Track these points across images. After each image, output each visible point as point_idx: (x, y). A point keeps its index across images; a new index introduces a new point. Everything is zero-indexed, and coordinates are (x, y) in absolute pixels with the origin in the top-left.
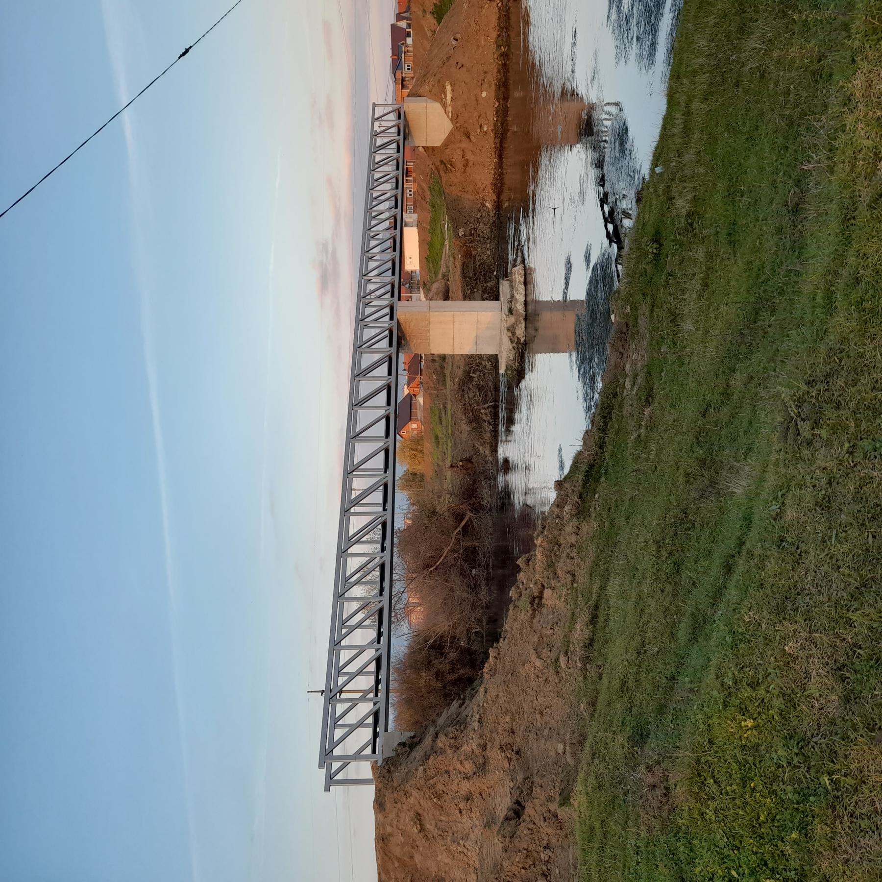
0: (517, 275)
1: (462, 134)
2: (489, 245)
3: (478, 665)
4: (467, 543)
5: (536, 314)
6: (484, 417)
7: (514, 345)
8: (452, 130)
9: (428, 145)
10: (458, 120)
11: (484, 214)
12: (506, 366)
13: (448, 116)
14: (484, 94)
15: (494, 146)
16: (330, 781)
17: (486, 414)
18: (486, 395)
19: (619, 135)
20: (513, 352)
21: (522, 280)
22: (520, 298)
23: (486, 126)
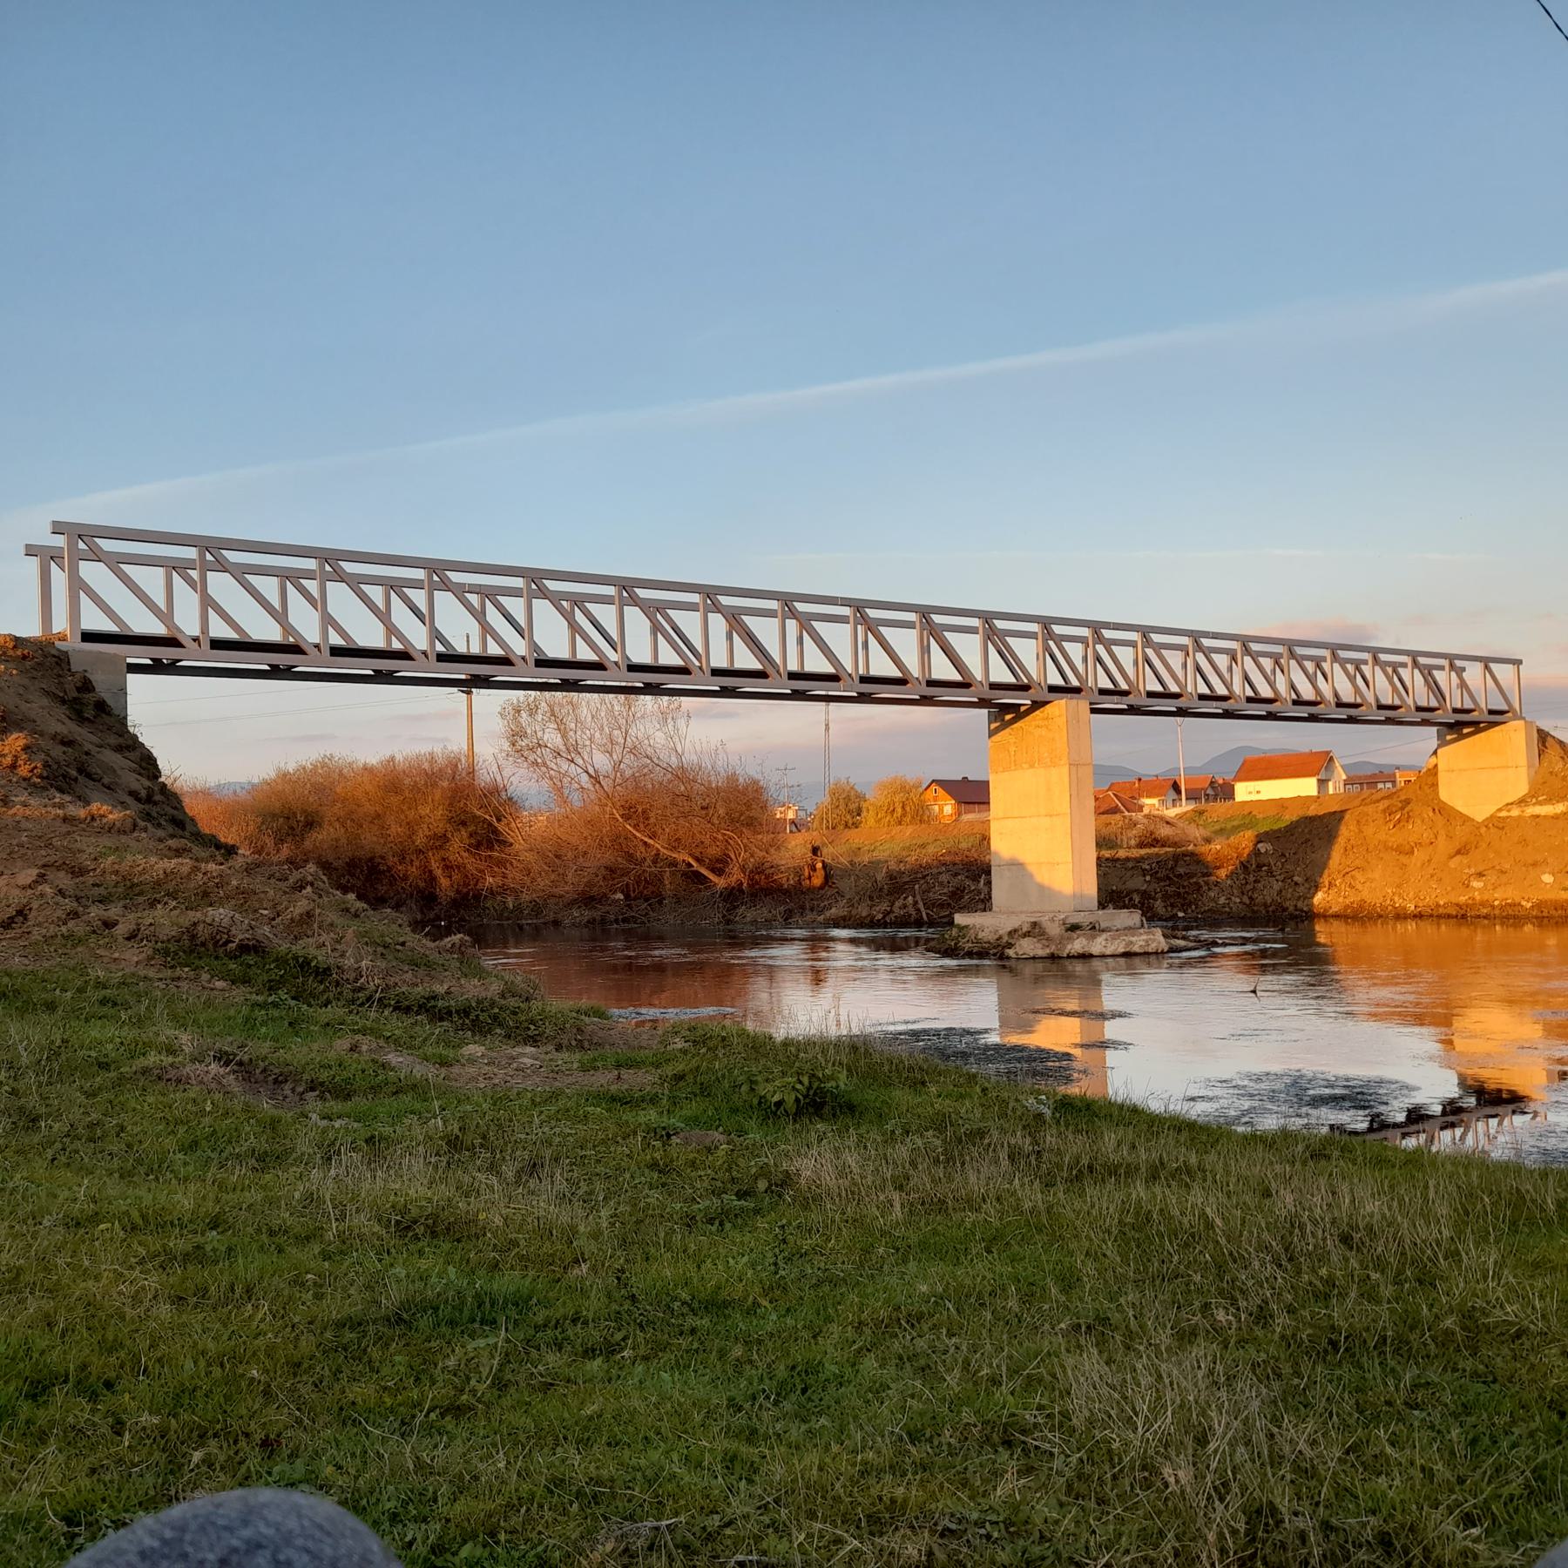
0: (1145, 937)
1: (1464, 839)
2: (1238, 900)
3: (458, 912)
5: (1068, 979)
7: (1006, 938)
9: (1440, 774)
10: (1493, 830)
11: (1301, 889)
12: (967, 927)
13: (1500, 810)
14: (1548, 878)
15: (1442, 903)
16: (46, 556)
17: (905, 906)
18: (942, 906)
19: (1362, 1093)
20: (992, 938)
21: (1136, 949)
22: (1098, 945)
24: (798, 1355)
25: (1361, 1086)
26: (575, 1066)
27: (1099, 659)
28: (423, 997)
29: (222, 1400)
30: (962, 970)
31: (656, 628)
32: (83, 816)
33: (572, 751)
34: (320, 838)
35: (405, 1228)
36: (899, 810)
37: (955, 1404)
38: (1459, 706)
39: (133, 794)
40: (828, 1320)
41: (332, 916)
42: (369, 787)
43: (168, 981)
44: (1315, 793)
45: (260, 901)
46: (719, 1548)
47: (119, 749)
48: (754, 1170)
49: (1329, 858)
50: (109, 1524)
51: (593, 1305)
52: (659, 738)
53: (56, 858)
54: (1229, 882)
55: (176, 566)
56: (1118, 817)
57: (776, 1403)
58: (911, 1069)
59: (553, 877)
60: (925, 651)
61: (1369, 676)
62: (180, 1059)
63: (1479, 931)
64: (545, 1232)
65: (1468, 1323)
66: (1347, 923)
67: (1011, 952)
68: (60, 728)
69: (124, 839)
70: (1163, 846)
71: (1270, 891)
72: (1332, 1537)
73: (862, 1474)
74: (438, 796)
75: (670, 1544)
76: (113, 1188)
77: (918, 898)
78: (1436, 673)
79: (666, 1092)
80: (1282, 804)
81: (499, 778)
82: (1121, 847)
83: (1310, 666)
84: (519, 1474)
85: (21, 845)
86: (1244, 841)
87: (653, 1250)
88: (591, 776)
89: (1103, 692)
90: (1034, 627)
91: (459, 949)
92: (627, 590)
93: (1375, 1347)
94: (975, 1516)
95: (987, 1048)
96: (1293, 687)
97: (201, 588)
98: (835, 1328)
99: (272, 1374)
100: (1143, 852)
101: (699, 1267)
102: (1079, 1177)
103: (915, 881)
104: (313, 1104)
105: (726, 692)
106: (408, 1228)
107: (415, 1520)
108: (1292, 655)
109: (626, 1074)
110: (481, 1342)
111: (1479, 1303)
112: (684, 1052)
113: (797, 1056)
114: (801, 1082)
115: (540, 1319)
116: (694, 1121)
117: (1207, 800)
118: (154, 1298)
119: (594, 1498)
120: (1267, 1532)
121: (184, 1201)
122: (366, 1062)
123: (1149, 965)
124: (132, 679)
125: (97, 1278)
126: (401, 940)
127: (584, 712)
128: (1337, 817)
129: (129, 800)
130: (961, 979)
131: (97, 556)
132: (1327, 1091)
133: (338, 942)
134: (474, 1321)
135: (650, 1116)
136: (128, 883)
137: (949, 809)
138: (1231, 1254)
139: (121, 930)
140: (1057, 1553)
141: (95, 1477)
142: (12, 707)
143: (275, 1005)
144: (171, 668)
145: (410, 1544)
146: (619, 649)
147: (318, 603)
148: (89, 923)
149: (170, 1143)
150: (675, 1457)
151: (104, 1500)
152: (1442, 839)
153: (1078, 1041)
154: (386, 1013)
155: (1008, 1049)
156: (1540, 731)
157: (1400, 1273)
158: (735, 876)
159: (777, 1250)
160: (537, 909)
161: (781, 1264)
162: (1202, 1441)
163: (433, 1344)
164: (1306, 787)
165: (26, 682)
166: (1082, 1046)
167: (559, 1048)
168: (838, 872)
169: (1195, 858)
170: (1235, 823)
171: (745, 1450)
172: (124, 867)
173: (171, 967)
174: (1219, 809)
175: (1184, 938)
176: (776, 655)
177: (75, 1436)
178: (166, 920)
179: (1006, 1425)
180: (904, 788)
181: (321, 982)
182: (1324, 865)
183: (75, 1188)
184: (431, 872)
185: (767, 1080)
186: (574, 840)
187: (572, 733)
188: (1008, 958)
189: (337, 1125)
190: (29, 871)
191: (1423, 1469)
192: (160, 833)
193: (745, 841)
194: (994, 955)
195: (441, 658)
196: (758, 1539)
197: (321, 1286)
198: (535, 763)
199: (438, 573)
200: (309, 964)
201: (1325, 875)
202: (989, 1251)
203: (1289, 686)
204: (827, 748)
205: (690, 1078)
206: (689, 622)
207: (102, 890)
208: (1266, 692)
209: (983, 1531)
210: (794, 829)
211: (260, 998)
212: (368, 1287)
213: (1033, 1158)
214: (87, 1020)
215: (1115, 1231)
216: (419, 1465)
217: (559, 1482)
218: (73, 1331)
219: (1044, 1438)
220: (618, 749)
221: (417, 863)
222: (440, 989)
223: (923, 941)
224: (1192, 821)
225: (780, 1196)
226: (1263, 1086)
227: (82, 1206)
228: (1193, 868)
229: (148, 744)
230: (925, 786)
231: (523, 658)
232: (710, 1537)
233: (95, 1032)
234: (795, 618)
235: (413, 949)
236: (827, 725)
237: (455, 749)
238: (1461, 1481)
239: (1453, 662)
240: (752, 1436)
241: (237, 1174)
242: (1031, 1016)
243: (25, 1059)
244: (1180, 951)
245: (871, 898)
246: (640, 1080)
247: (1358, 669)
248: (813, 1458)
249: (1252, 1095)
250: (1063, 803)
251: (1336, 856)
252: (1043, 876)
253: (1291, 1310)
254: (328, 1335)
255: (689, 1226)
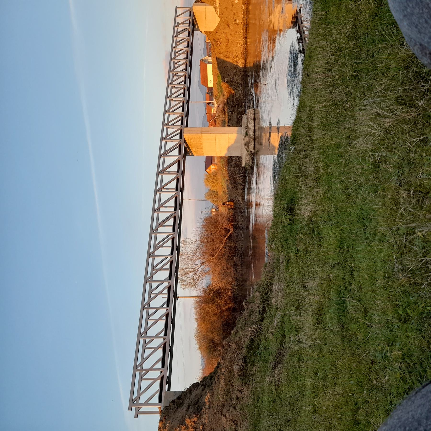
0: (250, 114)
2: (240, 88)
4: (232, 245)
5: (261, 136)
6: (239, 182)
7: (249, 153)
8: (220, 22)
10: (223, 16)
13: (217, 14)
16: (138, 412)
18: (240, 170)
19: (293, 57)
20: (249, 156)
21: (253, 117)
22: (252, 127)
23: (238, 20)
24: (354, 220)
25: (291, 57)
26: (278, 274)
27: (173, 125)
28: (259, 314)
29: (361, 374)
30: (257, 165)
31: (161, 246)
32: (208, 404)
33: (195, 270)
34: (216, 338)
35: (319, 322)
36: (213, 180)
37: (368, 180)
38: (188, 24)
39: (203, 390)
40: (346, 211)
41: (237, 338)
42: (203, 325)
43: (253, 382)
44: (211, 65)
45: (232, 357)
46: (402, 246)
47: (191, 393)
48: (307, 228)
49: (229, 62)
50: (391, 406)
51: (340, 274)
52: (192, 246)
53: (219, 411)
54: (235, 90)
55: (141, 377)
56: (217, 120)
57: (367, 227)
58: (282, 183)
59: (229, 276)
60: (169, 173)
61: (179, 49)
62: (273, 381)
63: (251, 21)
64: (321, 285)
65: (352, 39)
66: (247, 58)
67: (253, 151)
68: (185, 409)
69: (215, 393)
70: (225, 108)
71: (238, 79)
72: (405, 82)
73: (385, 206)
74: (205, 306)
75: (401, 259)
76: (306, 400)
77: (237, 176)
78: (179, 31)
79: (286, 250)
80: (214, 74)
81: (202, 290)
82: (225, 119)
83: (176, 66)
84: (382, 297)
85: (216, 421)
86: (224, 85)
87: (327, 257)
88: (202, 265)
89: (182, 124)
90: (164, 142)
91: (247, 304)
92: (151, 254)
93: (358, 65)
94: (396, 177)
95: (278, 160)
96: (182, 71)
97: (147, 370)
98: (348, 210)
99: (355, 361)
100: (226, 114)
101: (332, 245)
102: (312, 140)
103: (232, 176)
104: (286, 345)
105: (179, 228)
106: (319, 322)
107: (392, 325)
108: (173, 71)
109: (281, 260)
110: (348, 305)
111: (347, 35)
112: (276, 244)
113: (278, 214)
114: (284, 214)
115: (343, 288)
116: (294, 243)
117: (213, 95)
118: (334, 391)
119: (388, 278)
120: (403, 99)
121: (310, 381)
122: (276, 330)
123: (258, 113)
124: (172, 389)
125: (329, 406)
126: (244, 319)
127: (184, 266)
128: (218, 59)
129: (205, 391)
130: (260, 165)
131: (138, 398)
132: (292, 67)
133: (244, 336)
134: (343, 306)
135: (292, 254)
136: (227, 392)
137: (213, 166)
138: (332, 101)
139: (239, 395)
140: (406, 156)
141: (379, 409)
142: (179, 422)
143: (260, 354)
144: (169, 379)
145: (398, 327)
146: (162, 282)
147: (152, 338)
148: (237, 404)
149: (295, 384)
150: (379, 255)
151: (385, 407)
152: (225, 31)
153: (277, 134)
154: (263, 324)
155: (279, 154)
156: (196, 2)
157: (338, 56)
158: (230, 226)
159: (328, 224)
160: (238, 280)
161: (331, 223)
162: (379, 115)
163: (349, 317)
164: (210, 67)
165: (172, 418)
166: (278, 133)
167: (274, 278)
168: (230, 198)
169: (228, 99)
170: (219, 87)
171: (377, 238)
172: (222, 393)
173: (249, 381)
174: (215, 91)
175: (250, 103)
176: (170, 214)
177: (369, 414)
178: (237, 383)
179: (373, 167)
180: (207, 179)
181: (254, 341)
182: (232, 63)
183: (306, 410)
184: (227, 309)
185: (284, 222)
186: (219, 270)
187: (190, 270)
188: (254, 152)
189: (292, 339)
190: (223, 419)
191: (388, 56)
192: (214, 383)
193: (221, 223)
194: (253, 156)
195: (168, 305)
196: (400, 235)
197: (333, 346)
198: (198, 280)
199: (145, 306)
200: (249, 344)
201: (234, 63)
202: (330, 166)
203: (181, 72)
204: (195, 200)
205: (283, 243)
206: (160, 237)
207: (228, 400)
208: (183, 78)
209: (400, 175)
210: (218, 209)
211: (258, 358)
212: (334, 333)
213: (306, 152)
214: (263, 405)
215: (325, 132)
216: (379, 323)
217: (384, 287)
218: (342, 413)
219: (378, 157)
220: (195, 257)
221: (224, 313)
222: (257, 309)
223: (249, 175)
224: (218, 100)
225: (314, 221)
226: (290, 84)
227: (311, 409)
228: (231, 100)
229: (189, 386)
230: (207, 173)
231: (169, 283)
232: (399, 248)
233: (266, 403)
234: (159, 208)
235: (247, 316)
236: (189, 200)
237: (194, 301)
238: (392, 46)
239: (176, 26)
240: (375, 234)
241: (303, 367)
242: (270, 147)
243: (272, 422)
244: (254, 105)
245: (237, 189)
246: (283, 258)
247: (177, 52)
248: (380, 219)
249: (293, 88)
250: (212, 136)
251: (229, 60)
252: (232, 142)
253: (347, 87)
254: (345, 345)
255: (321, 246)
